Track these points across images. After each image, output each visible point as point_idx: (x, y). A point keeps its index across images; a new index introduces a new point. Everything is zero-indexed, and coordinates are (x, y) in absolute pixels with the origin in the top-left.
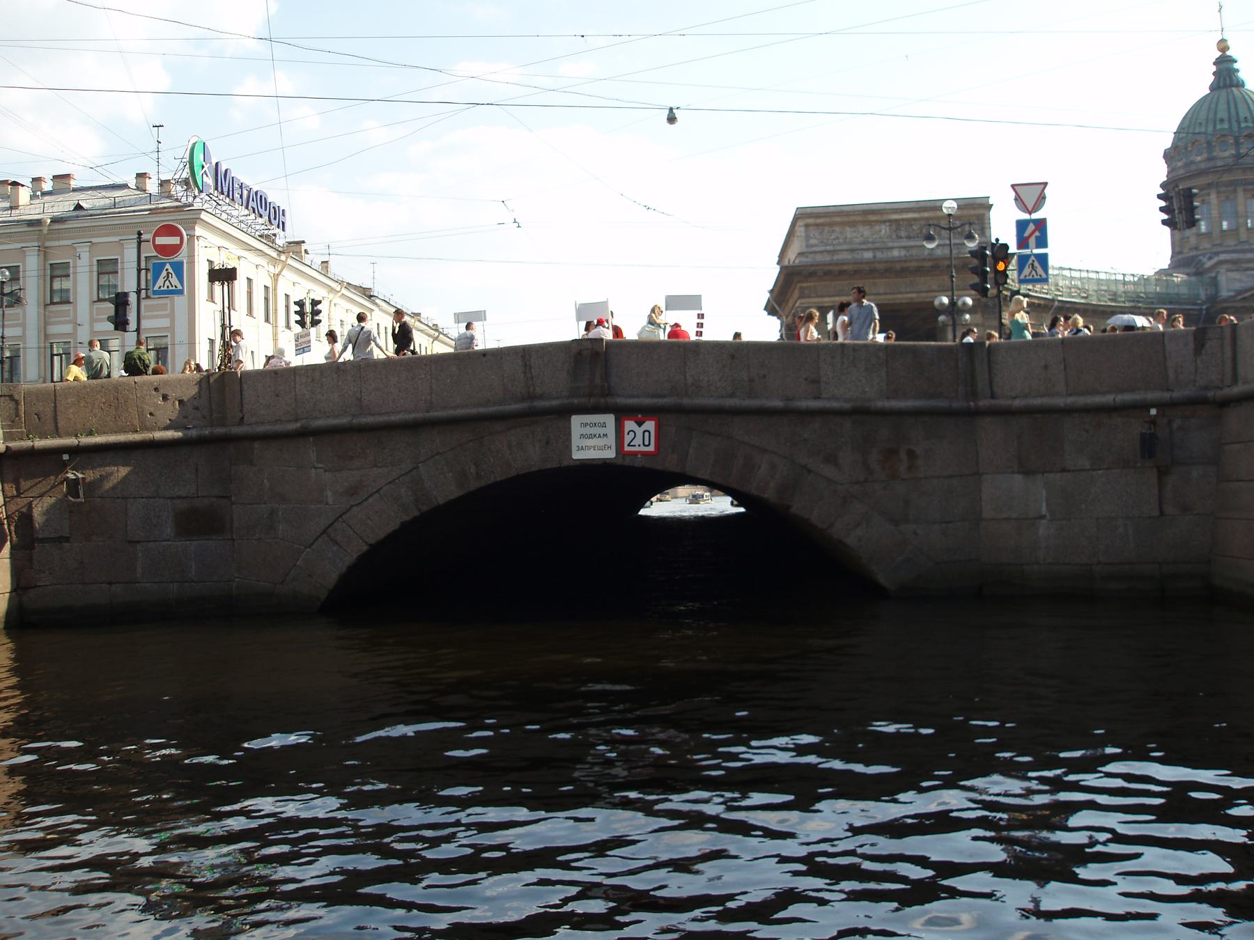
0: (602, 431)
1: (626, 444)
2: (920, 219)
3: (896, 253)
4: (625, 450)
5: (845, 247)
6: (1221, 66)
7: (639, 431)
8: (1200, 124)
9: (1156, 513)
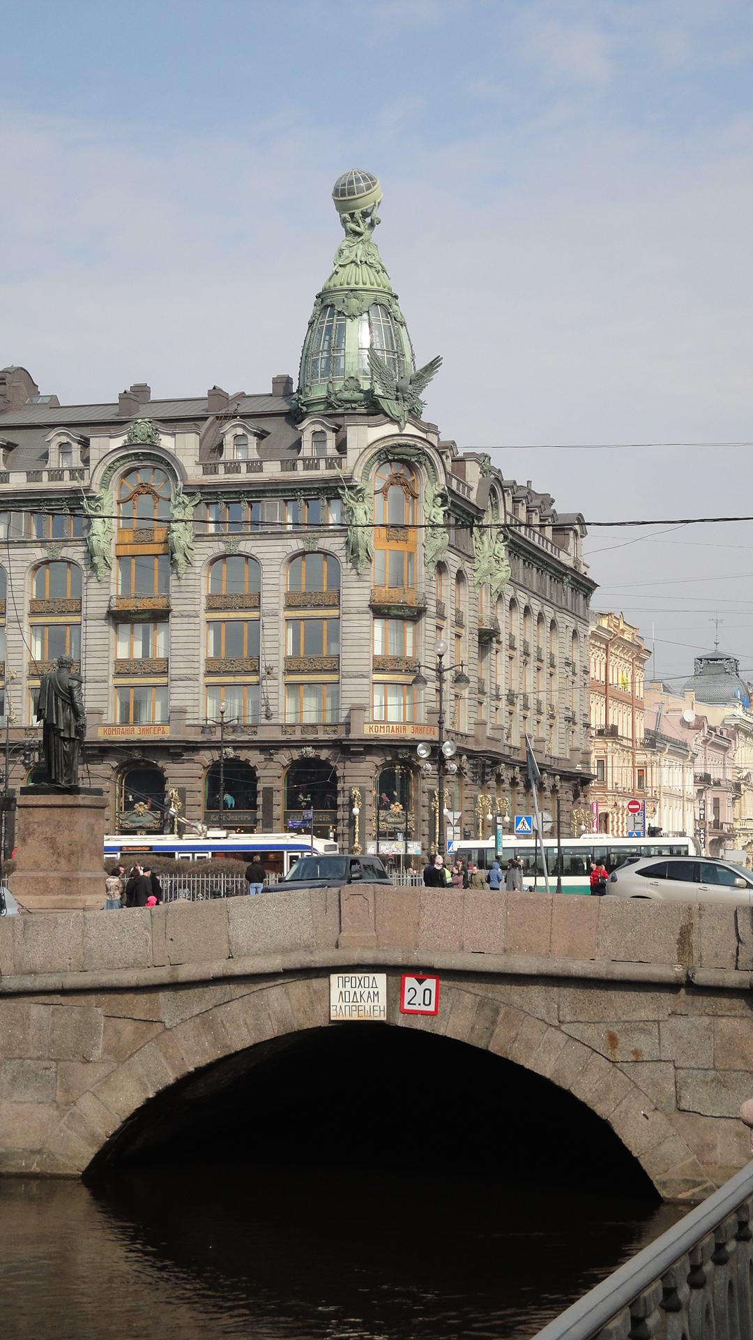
1: (406, 1001)
4: (405, 1008)
7: (420, 988)
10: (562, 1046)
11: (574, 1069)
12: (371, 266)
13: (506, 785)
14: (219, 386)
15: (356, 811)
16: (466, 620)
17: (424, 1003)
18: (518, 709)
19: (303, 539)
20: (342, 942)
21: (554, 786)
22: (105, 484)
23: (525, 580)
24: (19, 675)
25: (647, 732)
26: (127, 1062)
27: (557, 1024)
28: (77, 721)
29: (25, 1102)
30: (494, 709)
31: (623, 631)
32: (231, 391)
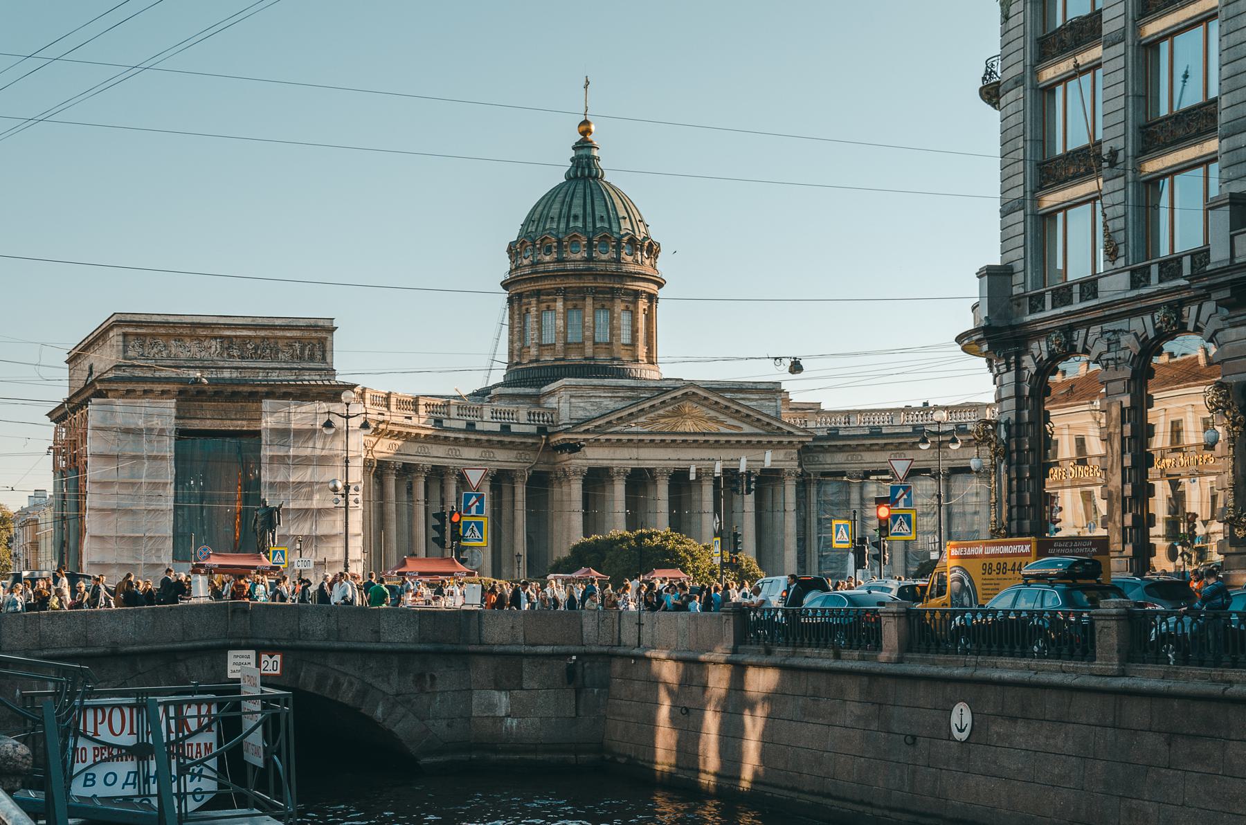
0: (247, 661)
2: (255, 337)
3: (226, 374)
5: (169, 363)
6: (581, 152)
7: (271, 661)
8: (552, 218)
9: (573, 715)
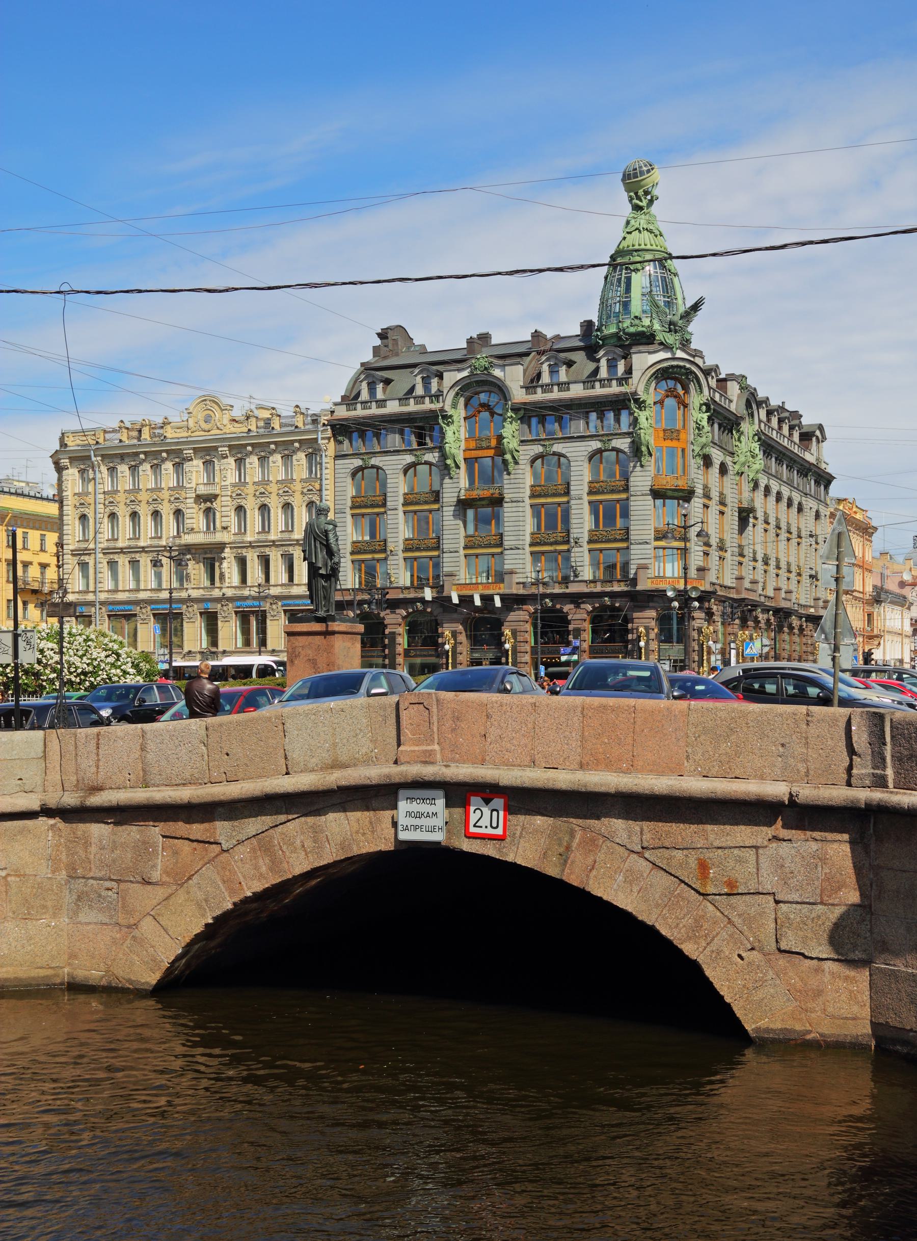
1: (472, 822)
10: (645, 875)
11: (660, 902)
12: (651, 231)
13: (796, 631)
14: (539, 329)
15: (642, 644)
16: (729, 500)
17: (491, 826)
18: (772, 569)
19: (600, 441)
20: (402, 759)
21: (801, 626)
22: (454, 406)
23: (777, 472)
24: (396, 549)
25: (875, 587)
26: (185, 885)
27: (640, 850)
28: (331, 559)
29: (90, 923)
30: (751, 568)
31: (855, 513)
32: (549, 334)
